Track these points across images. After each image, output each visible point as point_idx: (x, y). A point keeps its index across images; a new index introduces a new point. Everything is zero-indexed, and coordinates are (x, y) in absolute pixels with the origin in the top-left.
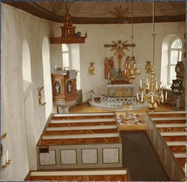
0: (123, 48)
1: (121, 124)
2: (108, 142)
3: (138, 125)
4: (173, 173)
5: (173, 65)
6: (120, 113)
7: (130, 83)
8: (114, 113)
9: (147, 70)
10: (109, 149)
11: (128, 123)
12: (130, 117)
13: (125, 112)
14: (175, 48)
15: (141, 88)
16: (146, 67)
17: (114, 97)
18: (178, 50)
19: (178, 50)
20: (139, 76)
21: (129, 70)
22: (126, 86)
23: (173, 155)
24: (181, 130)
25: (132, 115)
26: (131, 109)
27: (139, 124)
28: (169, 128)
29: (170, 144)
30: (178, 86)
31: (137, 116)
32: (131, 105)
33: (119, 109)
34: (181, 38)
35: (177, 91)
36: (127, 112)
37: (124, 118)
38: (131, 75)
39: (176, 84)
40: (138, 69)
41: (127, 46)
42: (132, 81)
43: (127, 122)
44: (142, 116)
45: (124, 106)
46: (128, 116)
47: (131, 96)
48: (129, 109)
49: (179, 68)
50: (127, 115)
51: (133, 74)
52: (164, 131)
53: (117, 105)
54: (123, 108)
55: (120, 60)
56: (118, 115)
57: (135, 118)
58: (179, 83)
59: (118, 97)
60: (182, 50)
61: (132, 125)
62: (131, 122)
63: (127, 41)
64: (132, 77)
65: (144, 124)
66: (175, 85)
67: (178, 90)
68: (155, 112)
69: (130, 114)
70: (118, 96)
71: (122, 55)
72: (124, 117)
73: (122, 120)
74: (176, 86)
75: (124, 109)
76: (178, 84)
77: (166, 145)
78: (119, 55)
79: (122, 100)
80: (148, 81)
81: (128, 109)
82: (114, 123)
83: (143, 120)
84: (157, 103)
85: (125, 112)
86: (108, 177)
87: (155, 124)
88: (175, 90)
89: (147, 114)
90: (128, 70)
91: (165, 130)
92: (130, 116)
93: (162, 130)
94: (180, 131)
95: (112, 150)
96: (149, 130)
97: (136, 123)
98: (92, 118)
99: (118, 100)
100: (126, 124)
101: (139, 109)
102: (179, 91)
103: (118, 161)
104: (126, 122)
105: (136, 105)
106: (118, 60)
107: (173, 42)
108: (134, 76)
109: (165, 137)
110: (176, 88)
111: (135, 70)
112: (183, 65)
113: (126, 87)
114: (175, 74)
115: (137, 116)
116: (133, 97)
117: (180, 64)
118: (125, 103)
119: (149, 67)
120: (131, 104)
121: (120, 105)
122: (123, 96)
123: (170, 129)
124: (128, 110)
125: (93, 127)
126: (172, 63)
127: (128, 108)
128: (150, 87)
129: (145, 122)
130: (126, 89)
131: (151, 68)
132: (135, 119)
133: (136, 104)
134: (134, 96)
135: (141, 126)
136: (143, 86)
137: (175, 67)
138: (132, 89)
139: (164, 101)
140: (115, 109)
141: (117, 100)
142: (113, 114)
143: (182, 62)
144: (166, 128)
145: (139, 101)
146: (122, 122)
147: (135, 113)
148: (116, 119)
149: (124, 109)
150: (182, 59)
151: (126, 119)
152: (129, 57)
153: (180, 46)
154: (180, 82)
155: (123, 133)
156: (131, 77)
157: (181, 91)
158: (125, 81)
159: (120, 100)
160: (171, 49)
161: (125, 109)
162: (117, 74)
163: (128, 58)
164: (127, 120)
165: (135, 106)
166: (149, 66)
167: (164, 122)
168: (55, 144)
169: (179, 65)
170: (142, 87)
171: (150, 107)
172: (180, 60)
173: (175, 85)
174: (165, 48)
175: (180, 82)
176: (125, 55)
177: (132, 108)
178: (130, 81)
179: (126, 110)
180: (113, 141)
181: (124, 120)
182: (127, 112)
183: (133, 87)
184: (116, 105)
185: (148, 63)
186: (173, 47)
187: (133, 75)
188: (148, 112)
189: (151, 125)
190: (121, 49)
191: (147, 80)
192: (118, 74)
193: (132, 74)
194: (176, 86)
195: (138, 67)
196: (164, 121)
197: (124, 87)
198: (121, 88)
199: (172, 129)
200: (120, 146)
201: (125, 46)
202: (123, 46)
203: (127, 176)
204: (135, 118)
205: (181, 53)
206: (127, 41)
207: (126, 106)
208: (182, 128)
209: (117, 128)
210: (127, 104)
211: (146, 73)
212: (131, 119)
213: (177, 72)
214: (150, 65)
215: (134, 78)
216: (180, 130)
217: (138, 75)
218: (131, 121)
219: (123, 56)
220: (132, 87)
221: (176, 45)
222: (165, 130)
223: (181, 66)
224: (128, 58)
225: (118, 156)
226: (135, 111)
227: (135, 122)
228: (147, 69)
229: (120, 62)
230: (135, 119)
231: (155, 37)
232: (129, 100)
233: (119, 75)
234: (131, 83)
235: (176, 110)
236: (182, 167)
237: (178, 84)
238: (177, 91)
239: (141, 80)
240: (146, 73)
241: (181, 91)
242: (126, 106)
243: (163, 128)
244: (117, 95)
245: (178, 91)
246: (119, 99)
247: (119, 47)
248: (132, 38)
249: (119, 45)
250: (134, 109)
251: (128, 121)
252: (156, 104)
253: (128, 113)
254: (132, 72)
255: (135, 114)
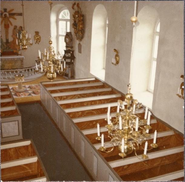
0: (10, 17)
1: (15, 97)
2: (5, 116)
3: (32, 96)
4: (73, 137)
5: (62, 36)
6: (12, 85)
7: (20, 55)
8: (6, 85)
9: (36, 40)
10: (8, 123)
11: (22, 95)
12: (23, 89)
13: (18, 85)
14: (63, 18)
15: (40, 58)
16: (35, 37)
17: (4, 69)
18: (66, 20)
19: (66, 20)
20: (32, 46)
21: (20, 40)
22: (15, 57)
23: (72, 120)
24: (75, 97)
25: (25, 87)
26: (23, 81)
27: (33, 95)
28: (64, 96)
29: (68, 111)
30: (70, 56)
31: (29, 87)
32: (24, 77)
33: (9, 81)
34: (69, 9)
35: (69, 61)
36: (20, 85)
37: (17, 91)
38: (23, 45)
39: (68, 54)
40: (30, 39)
41: (14, 14)
42: (21, 52)
43: (20, 94)
44: (35, 87)
45: (16, 78)
46: (21, 88)
47: (22, 68)
48: (22, 80)
49: (68, 38)
50: (20, 87)
51: (26, 44)
52: (60, 99)
53: (8, 78)
54: (15, 81)
55: (7, 29)
56: (10, 87)
57: (28, 89)
58: (70, 53)
59: (8, 69)
60: (70, 20)
61: (27, 96)
62: (25, 94)
63: (13, 10)
64: (24, 47)
65: (38, 94)
66: (67, 55)
67: (70, 60)
68: (54, 82)
69: (23, 86)
70: (7, 69)
71: (8, 24)
72: (17, 90)
73: (15, 93)
74: (68, 56)
75: (17, 81)
76: (70, 54)
77: (64, 112)
78: (5, 25)
79: (13, 72)
80: (46, 50)
81: (21, 81)
82: (9, 96)
83: (36, 91)
84: (57, 73)
85: (18, 85)
86: (12, 150)
87: (51, 94)
88: (66, 60)
89: (42, 84)
90: (19, 40)
91: (61, 98)
92: (23, 88)
93: (58, 98)
94: (74, 98)
95: (11, 123)
96: (45, 100)
97: (30, 95)
98: (67, 85)
99: (8, 72)
100: (20, 96)
101: (31, 80)
102: (71, 61)
103: (18, 133)
104: (19, 95)
105: (27, 77)
106: (5, 29)
107: (60, 13)
108: (26, 47)
109: (61, 105)
110: (68, 58)
111: (27, 40)
112: (72, 35)
113: (16, 58)
114: (65, 44)
115: (29, 87)
116: (24, 68)
117: (69, 35)
118: (17, 75)
119: (38, 37)
120: (23, 75)
121: (11, 77)
122: (13, 68)
123: (65, 97)
124: (20, 82)
125: (65, 93)
126: (60, 33)
127: (21, 80)
128: (49, 57)
129: (39, 93)
130: (15, 61)
131: (41, 37)
132: (29, 90)
133: (27, 76)
134: (24, 67)
135: (36, 97)
136: (42, 56)
137: (64, 38)
138: (22, 60)
139: (63, 70)
140: (7, 81)
141: (11, 73)
142: (6, 87)
143: (70, 33)
144: (62, 97)
145: (38, 71)
146: (16, 95)
147: (27, 84)
148: (11, 92)
149: (17, 81)
150: (70, 30)
151: (19, 91)
152: (16, 27)
153: (68, 16)
154: (71, 52)
155: (20, 105)
156: (24, 48)
157: (73, 60)
158: (13, 52)
159: (10, 73)
160: (59, 19)
161: (17, 81)
162: (5, 45)
163: (15, 27)
164: (20, 92)
165: (28, 78)
166: (37, 36)
167: (59, 91)
168: (87, 112)
169: (68, 35)
170: (41, 58)
171: (49, 77)
172: (68, 31)
173: (67, 55)
174: (53, 18)
175: (71, 52)
176: (12, 25)
177: (25, 80)
178: (20, 53)
179: (19, 82)
180: (10, 114)
181: (17, 92)
182: (20, 85)
183: (23, 58)
184: (6, 77)
185: (37, 33)
186: (60, 17)
187: (25, 46)
188: (42, 82)
189: (47, 95)
190: (7, 18)
191: (45, 50)
192: (6, 44)
193: (25, 44)
194: (68, 56)
195: (30, 37)
196: (59, 90)
197: (13, 58)
198: (10, 60)
199: (67, 98)
200: (19, 118)
201: (12, 15)
202: (9, 14)
203: (31, 146)
204: (28, 89)
205: (69, 23)
206: (13, 10)
207: (19, 78)
208: (76, 96)
209: (13, 101)
210: (19, 76)
211: (36, 43)
212: (24, 90)
213: (67, 43)
214: (39, 35)
215: (25, 49)
216: (74, 97)
217: (31, 45)
218: (24, 93)
219: (10, 25)
220: (22, 58)
221: (64, 15)
222: (61, 98)
223: (70, 36)
224: (15, 27)
225: (18, 128)
226: (28, 83)
227: (28, 94)
228: (36, 40)
229: (7, 32)
230: (29, 90)
231: (52, 5)
232: (20, 72)
233: (7, 45)
234: (21, 55)
235: (69, 79)
236: (81, 131)
237: (70, 54)
238: (69, 61)
239: (30, 52)
240: (36, 43)
241: (73, 60)
242: (18, 78)
243: (59, 97)
244: (6, 67)
245: (70, 61)
246: (9, 71)
247: (5, 15)
248: (21, 7)
249: (5, 13)
250: (26, 81)
251: (22, 94)
252: (55, 74)
253: (20, 84)
254: (25, 42)
255: (27, 86)
